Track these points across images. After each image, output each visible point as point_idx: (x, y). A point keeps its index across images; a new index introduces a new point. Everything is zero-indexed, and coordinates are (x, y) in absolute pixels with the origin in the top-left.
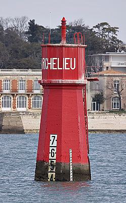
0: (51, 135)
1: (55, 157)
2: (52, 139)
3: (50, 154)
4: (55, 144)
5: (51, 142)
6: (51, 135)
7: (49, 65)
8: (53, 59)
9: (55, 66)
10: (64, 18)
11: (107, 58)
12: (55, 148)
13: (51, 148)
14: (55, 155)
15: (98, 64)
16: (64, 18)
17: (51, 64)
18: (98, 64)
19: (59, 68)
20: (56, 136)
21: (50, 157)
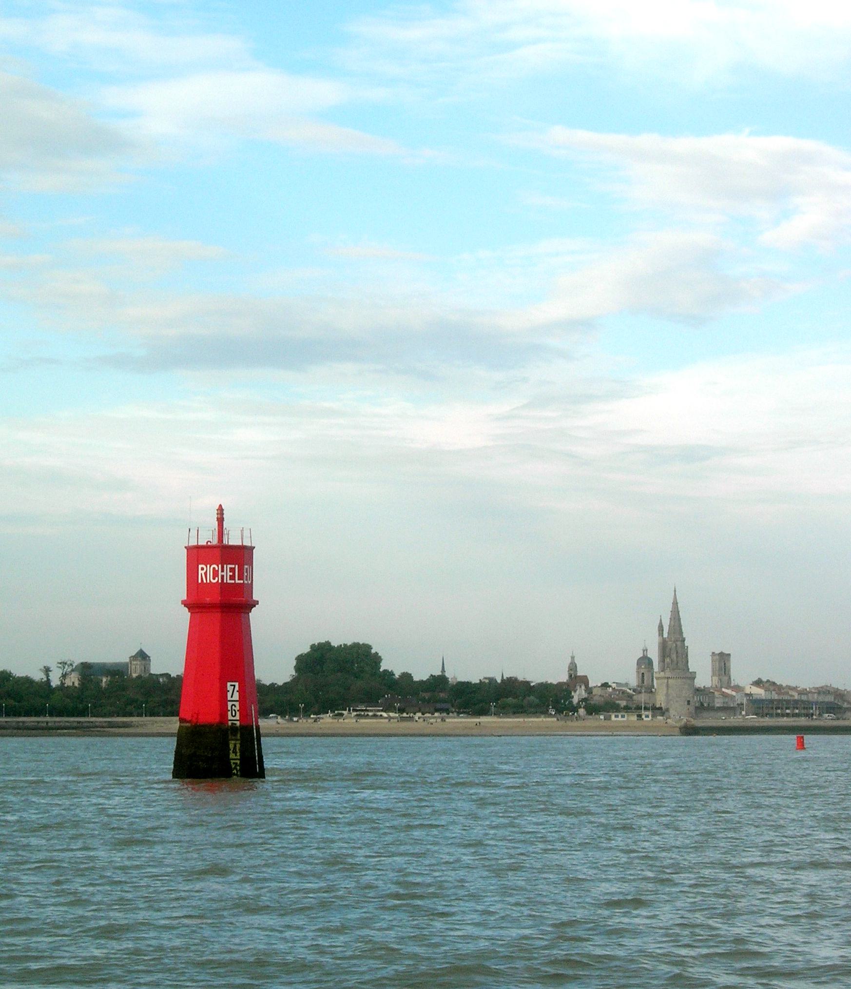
0: (229, 684)
1: (237, 717)
2: (230, 689)
3: (230, 713)
4: (236, 696)
5: (229, 694)
6: (229, 684)
7: (222, 576)
8: (229, 566)
9: (232, 577)
10: (220, 506)
11: (705, 851)
12: (237, 704)
13: (230, 704)
14: (238, 713)
15: (199, 903)
16: (220, 506)
17: (224, 573)
18: (199, 903)
19: (237, 581)
20: (237, 684)
21: (230, 717)
